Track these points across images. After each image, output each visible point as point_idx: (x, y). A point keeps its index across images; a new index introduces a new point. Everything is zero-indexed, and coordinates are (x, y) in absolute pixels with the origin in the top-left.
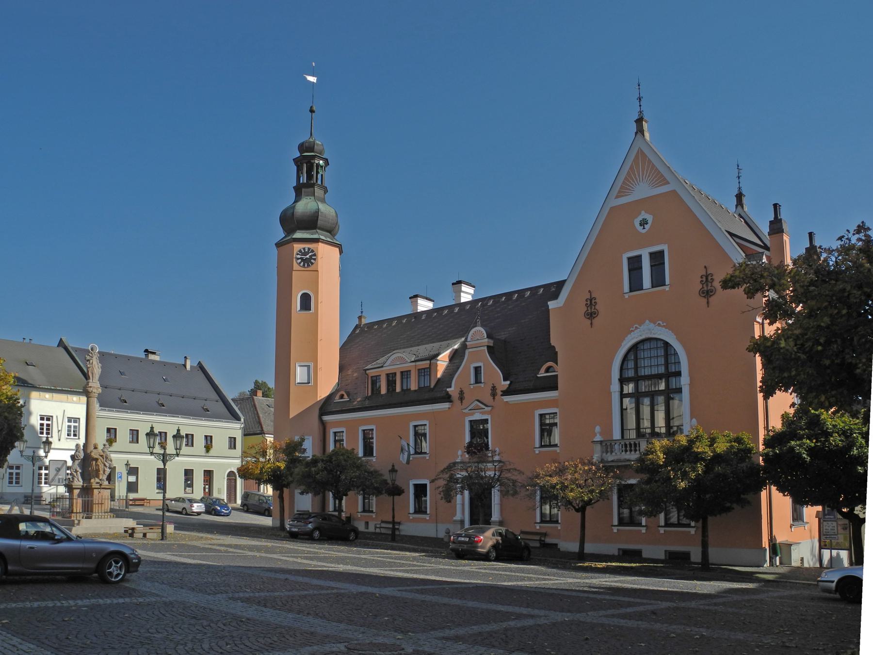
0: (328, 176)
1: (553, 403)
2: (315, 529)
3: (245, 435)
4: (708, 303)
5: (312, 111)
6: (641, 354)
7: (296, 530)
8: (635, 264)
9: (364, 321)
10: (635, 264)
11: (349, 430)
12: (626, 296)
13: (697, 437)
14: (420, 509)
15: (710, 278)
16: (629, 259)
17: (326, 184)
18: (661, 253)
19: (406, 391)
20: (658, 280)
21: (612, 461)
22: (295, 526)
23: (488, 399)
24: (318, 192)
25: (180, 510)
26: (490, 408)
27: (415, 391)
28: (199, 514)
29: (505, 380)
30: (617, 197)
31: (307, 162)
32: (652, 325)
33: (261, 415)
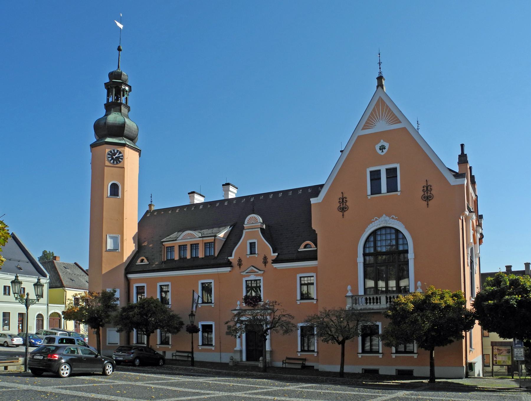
0: (131, 99)
1: (314, 269)
2: (137, 358)
3: (50, 287)
4: (428, 204)
5: (119, 49)
6: (379, 238)
7: (121, 359)
8: (375, 176)
9: (153, 208)
10: (375, 176)
11: (153, 284)
12: (369, 197)
13: (432, 293)
14: (207, 342)
15: (345, 200)
16: (371, 172)
17: (129, 104)
18: (395, 169)
19: (183, 259)
20: (392, 187)
21: (361, 310)
22: (120, 356)
23: (261, 266)
24: (124, 110)
25: (2, 343)
26: (262, 272)
27: (202, 258)
28: (17, 346)
29: (274, 252)
30: (363, 129)
31: (115, 86)
32: (387, 218)
33: (60, 274)
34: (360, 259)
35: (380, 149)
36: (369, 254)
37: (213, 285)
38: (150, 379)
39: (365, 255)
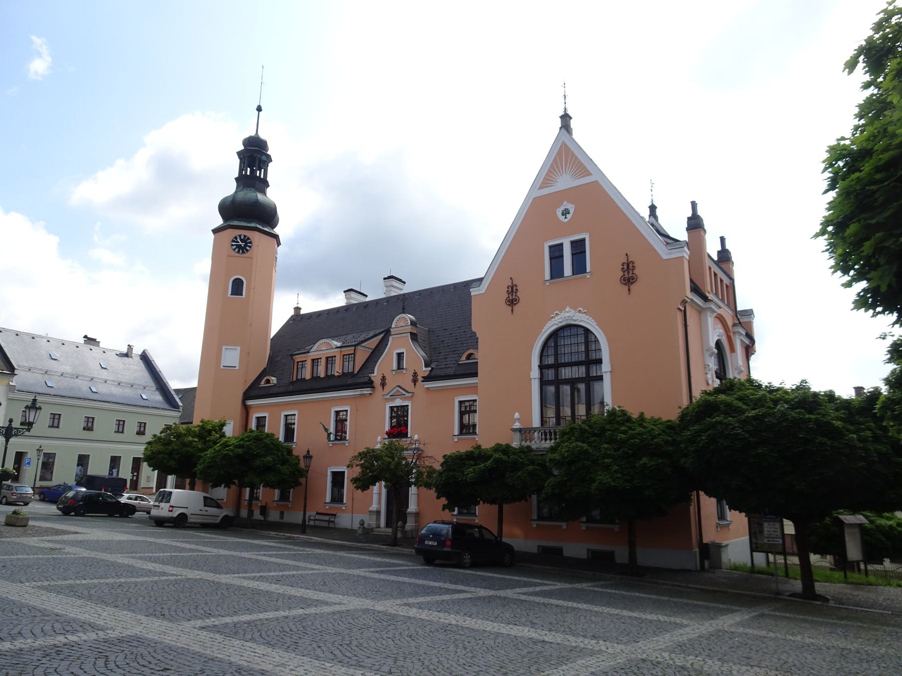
6: (562, 342)
8: (556, 253)
18: (583, 240)
20: (579, 267)
23: (409, 386)
29: (426, 366)
34: (535, 373)
35: (563, 214)
36: (549, 367)
37: (410, 407)
38: (262, 548)
39: (542, 367)
